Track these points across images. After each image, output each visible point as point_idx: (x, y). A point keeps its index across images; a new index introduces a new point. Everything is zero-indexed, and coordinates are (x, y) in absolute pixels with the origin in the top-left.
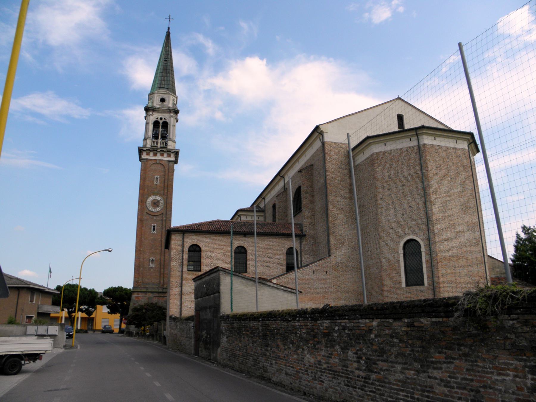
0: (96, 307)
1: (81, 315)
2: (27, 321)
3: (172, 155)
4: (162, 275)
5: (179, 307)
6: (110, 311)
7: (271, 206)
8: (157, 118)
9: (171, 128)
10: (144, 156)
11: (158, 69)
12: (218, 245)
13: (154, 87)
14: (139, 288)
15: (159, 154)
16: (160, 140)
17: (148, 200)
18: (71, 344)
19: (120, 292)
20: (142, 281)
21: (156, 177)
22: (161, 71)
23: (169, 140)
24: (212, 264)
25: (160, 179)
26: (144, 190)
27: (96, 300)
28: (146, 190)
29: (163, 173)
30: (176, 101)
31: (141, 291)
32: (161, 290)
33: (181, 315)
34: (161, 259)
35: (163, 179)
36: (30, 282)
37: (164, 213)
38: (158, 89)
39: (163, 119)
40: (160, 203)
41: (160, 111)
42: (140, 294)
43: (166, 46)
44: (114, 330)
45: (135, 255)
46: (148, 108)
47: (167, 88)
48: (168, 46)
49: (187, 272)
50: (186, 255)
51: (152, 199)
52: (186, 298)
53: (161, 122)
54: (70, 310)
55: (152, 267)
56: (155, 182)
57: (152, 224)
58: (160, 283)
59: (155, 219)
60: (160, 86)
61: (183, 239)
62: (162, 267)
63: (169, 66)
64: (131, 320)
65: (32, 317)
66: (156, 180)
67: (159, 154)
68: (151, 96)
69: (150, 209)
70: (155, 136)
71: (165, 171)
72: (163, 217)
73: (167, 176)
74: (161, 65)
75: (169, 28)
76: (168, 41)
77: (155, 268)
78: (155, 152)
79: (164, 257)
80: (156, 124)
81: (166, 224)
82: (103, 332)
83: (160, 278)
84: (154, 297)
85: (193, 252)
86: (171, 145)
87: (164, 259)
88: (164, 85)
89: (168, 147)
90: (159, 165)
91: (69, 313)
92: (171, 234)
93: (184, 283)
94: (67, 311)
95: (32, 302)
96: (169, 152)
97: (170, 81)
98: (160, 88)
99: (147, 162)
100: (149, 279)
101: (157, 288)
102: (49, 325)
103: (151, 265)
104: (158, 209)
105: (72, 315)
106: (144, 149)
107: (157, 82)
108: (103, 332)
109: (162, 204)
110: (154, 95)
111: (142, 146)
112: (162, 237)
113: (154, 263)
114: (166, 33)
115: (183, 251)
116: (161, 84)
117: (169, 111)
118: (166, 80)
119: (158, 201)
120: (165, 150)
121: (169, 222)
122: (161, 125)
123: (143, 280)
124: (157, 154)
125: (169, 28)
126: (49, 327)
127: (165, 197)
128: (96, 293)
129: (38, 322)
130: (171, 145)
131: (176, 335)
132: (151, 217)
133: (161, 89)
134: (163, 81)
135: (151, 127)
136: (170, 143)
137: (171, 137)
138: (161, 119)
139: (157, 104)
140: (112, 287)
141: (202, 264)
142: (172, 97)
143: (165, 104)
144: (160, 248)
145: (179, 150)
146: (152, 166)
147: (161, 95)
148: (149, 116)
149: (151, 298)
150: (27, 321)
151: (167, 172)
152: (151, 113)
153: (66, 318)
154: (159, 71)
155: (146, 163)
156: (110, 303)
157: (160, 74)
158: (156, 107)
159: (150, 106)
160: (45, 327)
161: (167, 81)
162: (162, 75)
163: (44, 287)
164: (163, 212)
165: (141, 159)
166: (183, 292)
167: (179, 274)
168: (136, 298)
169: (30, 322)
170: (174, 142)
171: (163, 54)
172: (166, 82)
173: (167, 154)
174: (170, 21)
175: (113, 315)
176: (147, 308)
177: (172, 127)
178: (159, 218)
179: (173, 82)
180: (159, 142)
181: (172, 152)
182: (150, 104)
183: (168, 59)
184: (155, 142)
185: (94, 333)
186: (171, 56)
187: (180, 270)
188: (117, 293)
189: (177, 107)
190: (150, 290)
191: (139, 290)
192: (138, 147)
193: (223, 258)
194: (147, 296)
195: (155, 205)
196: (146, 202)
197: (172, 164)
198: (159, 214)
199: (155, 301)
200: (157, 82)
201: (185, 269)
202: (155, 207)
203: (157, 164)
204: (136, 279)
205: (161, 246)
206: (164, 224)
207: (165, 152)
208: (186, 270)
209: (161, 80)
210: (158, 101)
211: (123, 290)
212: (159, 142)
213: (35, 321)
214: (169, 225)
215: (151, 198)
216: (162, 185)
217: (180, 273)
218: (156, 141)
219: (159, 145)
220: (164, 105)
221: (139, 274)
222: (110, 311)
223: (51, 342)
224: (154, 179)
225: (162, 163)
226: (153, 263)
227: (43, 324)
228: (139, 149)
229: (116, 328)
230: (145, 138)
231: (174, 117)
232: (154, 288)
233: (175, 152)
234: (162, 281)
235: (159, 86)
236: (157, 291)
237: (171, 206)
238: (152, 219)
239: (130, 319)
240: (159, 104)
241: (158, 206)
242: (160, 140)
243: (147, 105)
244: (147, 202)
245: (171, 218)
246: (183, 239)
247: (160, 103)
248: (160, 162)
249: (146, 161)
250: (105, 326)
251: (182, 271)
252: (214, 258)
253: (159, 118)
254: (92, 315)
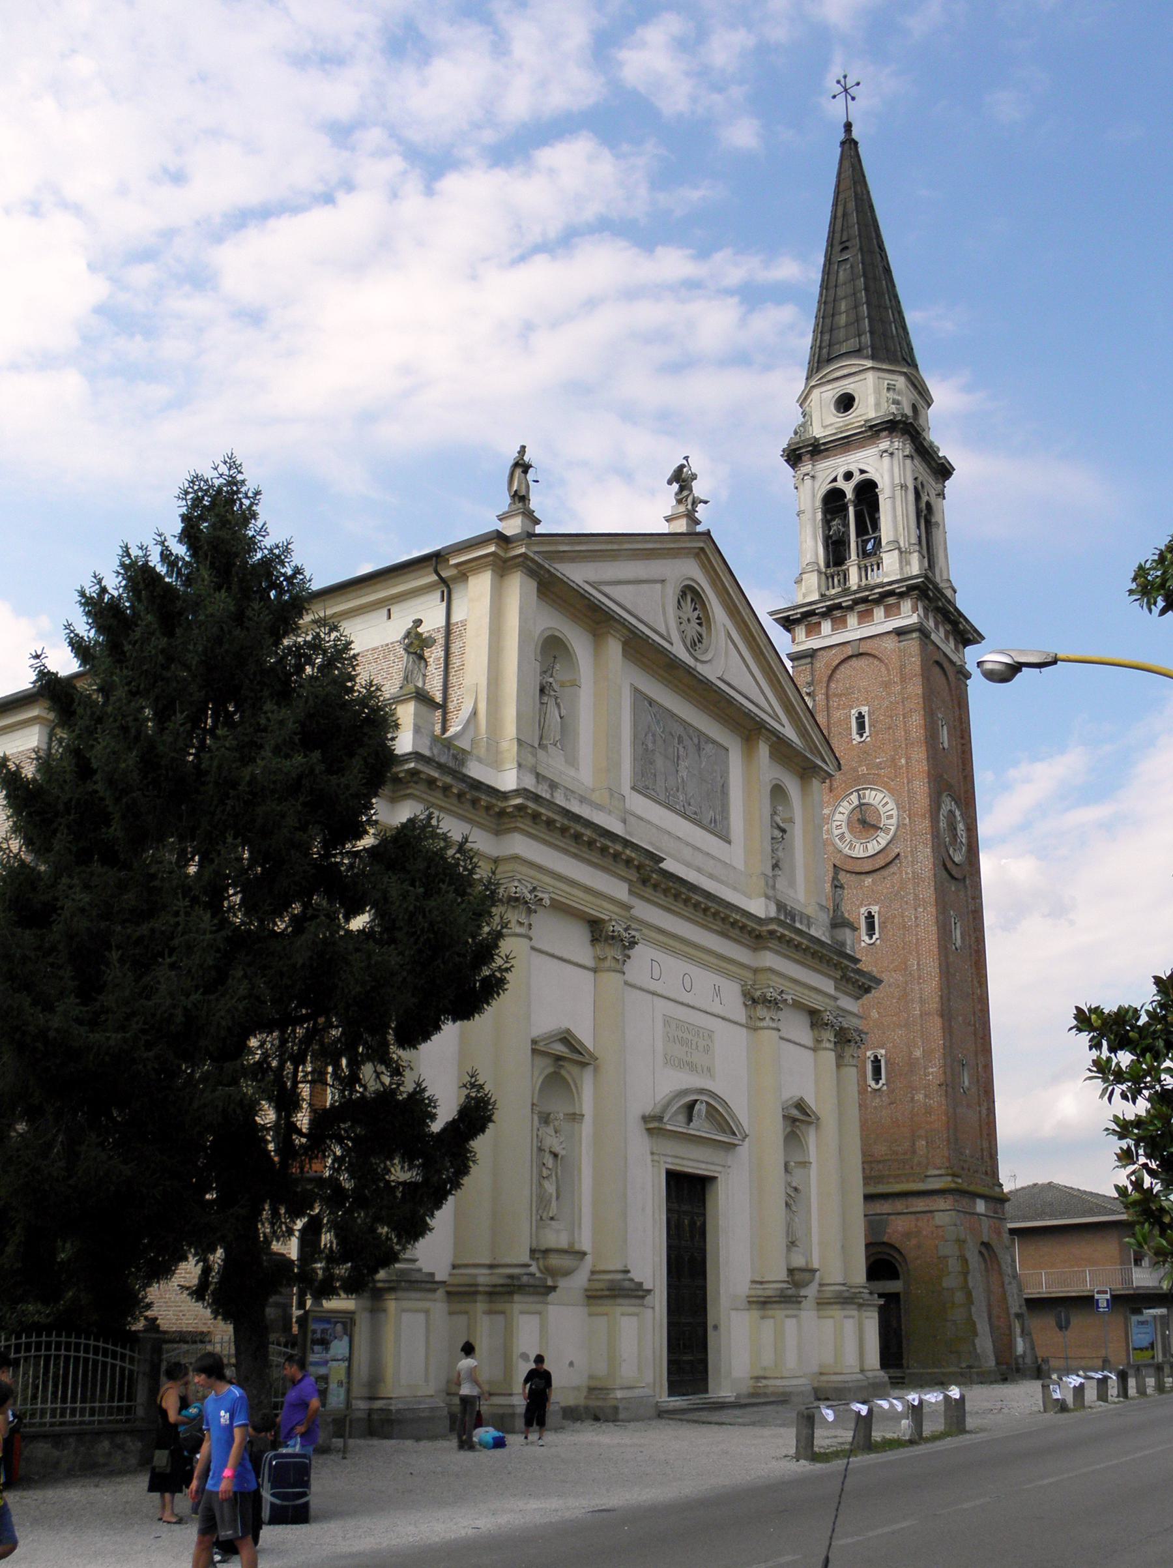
8: (835, 480)
53: (848, 488)
72: (829, 354)
80: (833, 501)
125: (848, 127)
138: (848, 476)
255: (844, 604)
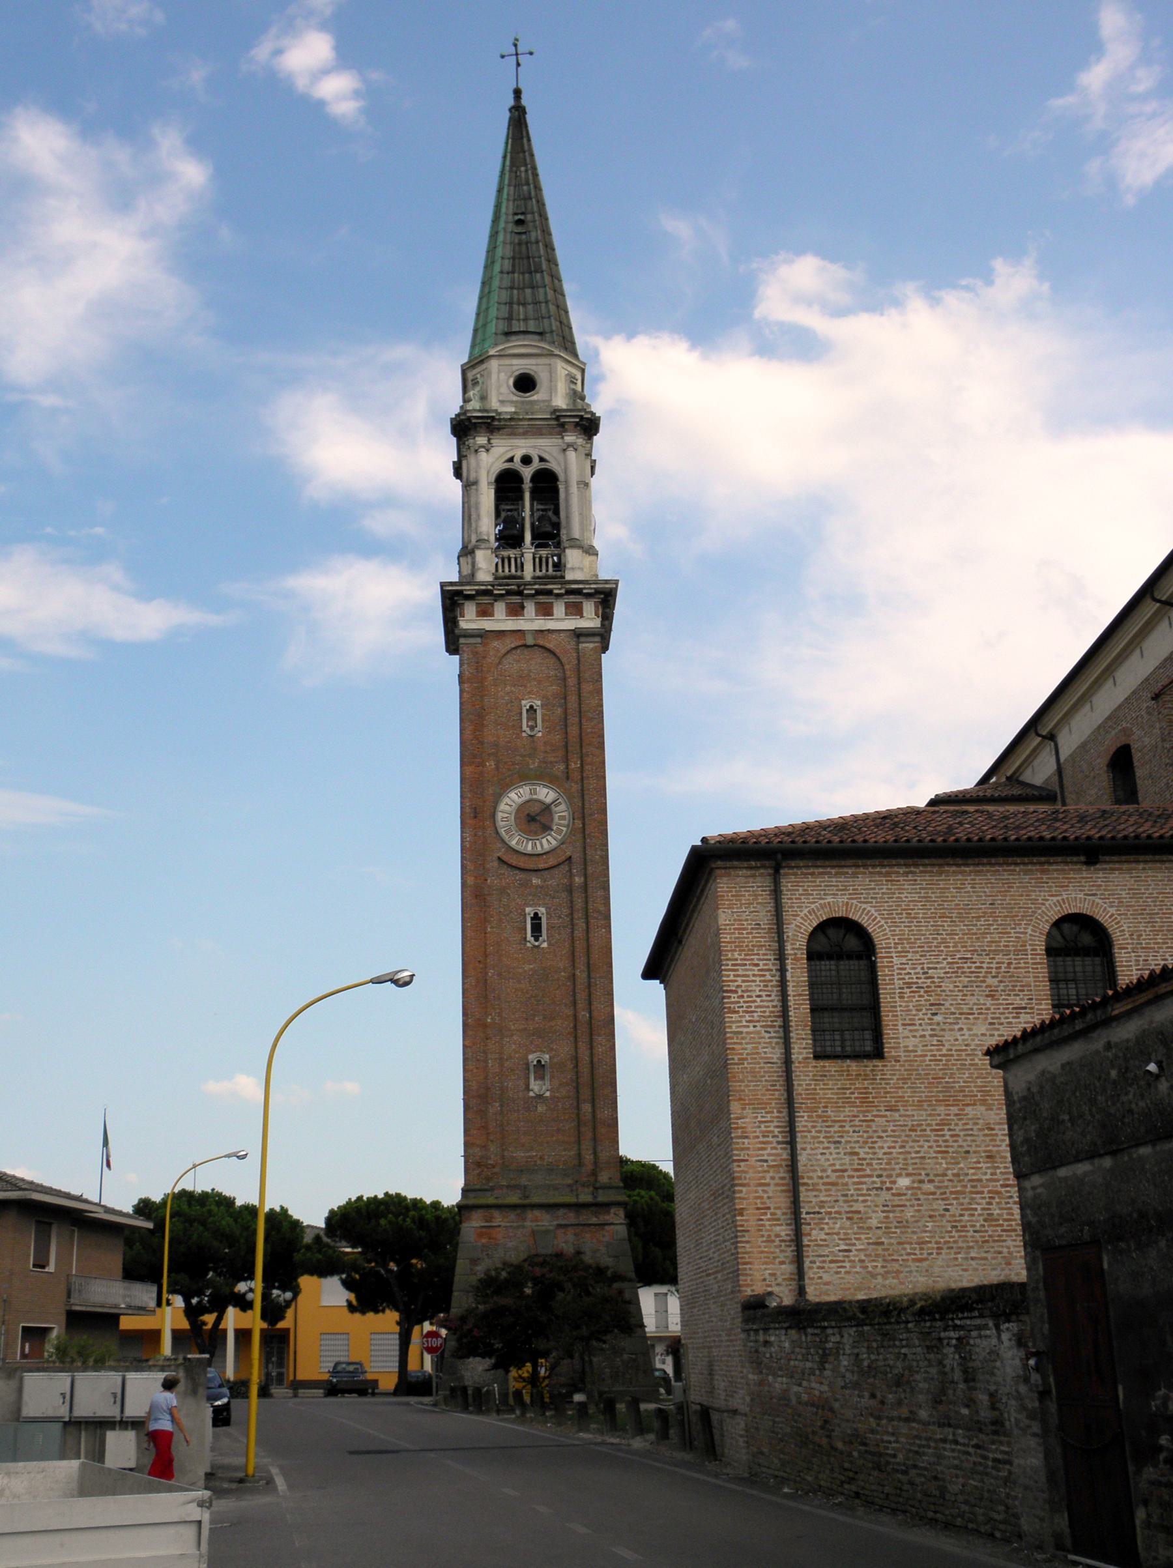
0: (298, 1286)
1: (236, 1321)
2: (27, 1350)
3: (589, 607)
4: (587, 1132)
5: (790, 1252)
6: (357, 1298)
7: (1102, 762)
8: (511, 460)
9: (570, 495)
10: (469, 620)
11: (493, 262)
12: (960, 916)
13: (484, 333)
14: (492, 1189)
15: (530, 608)
16: (528, 550)
17: (502, 806)
18: (239, 1461)
19: (397, 1216)
20: (503, 1157)
21: (526, 704)
22: (507, 265)
23: (571, 547)
24: (938, 1018)
25: (543, 715)
26: (482, 764)
27: (297, 1257)
28: (490, 764)
29: (555, 688)
30: (579, 382)
31: (500, 1202)
32: (586, 1197)
33: (801, 1291)
34: (576, 1059)
35: (559, 711)
36: (32, 1183)
37: (577, 857)
38: (503, 338)
39: (536, 460)
40: (556, 816)
41: (521, 431)
42: (498, 1219)
43: (512, 164)
44: (376, 1381)
45: (465, 1046)
46: (469, 419)
47: (540, 334)
48: (526, 165)
49: (814, 1063)
50: (798, 974)
51: (520, 801)
52: (822, 1204)
53: (527, 473)
54: (194, 1301)
55: (540, 1097)
56: (525, 727)
57: (528, 910)
58: (580, 1164)
59: (537, 886)
60: (510, 325)
61: (776, 893)
62: (585, 1093)
63: (537, 242)
64: (476, 1332)
65: (45, 1331)
66: (528, 719)
67: (530, 608)
68: (475, 371)
69: (513, 843)
70: (509, 538)
71: (565, 679)
72: (571, 876)
73: (573, 699)
74: (504, 243)
75: (517, 93)
76: (522, 145)
77: (552, 1097)
78: (516, 599)
79: (591, 1048)
80: (507, 484)
81: (587, 903)
82: (332, 1390)
83: (579, 1142)
84: (560, 1226)
85: (830, 957)
86: (576, 567)
87: (592, 1054)
88: (526, 319)
89: (569, 576)
90: (538, 656)
91: (192, 1312)
92: (712, 870)
93: (803, 1121)
94: (183, 1305)
95: (43, 1267)
96: (576, 595)
97: (547, 302)
98: (508, 334)
99: (484, 644)
100: (532, 1149)
101: (569, 1185)
102: (128, 1369)
103: (535, 1086)
104: (547, 842)
105: (205, 1323)
106: (469, 589)
107: (493, 312)
108: (332, 1390)
109: (563, 818)
110: (483, 366)
111: (455, 578)
112: (573, 961)
113: (547, 1077)
114: (508, 115)
115: (781, 957)
116: (510, 319)
117: (558, 422)
118: (529, 299)
119: (547, 809)
120: (557, 589)
121: (600, 893)
122: (527, 486)
123: (506, 1153)
124: (523, 607)
125: (517, 93)
126: (131, 1376)
127: (575, 787)
128: (296, 1224)
129: (73, 1353)
130: (576, 567)
131: (822, 1405)
132: (522, 875)
133: (513, 338)
134: (519, 304)
135: (487, 497)
136: (573, 557)
137: (576, 534)
138: (526, 460)
139: (502, 402)
140: (360, 1198)
141: (887, 1018)
142: (562, 369)
143: (535, 398)
144: (569, 1012)
145: (616, 582)
146: (510, 658)
147: (515, 361)
148: (476, 451)
149: (547, 1232)
150: (27, 1350)
151: (572, 682)
152: (481, 440)
153: (177, 1335)
154: (497, 268)
155: (480, 649)
156: (354, 1267)
157: (501, 279)
158: (500, 414)
159: (475, 410)
160: (109, 1380)
161: (536, 303)
162: (513, 281)
163: (86, 1201)
164: (568, 854)
165: (453, 641)
166: (801, 1168)
167: (771, 1074)
168: (480, 1235)
169: (37, 1352)
170: (591, 551)
171: (505, 196)
172: (530, 307)
173: (567, 605)
174: (518, 65)
175: (370, 1315)
176: (543, 1275)
177: (574, 489)
178: (556, 880)
179: (562, 309)
180: (528, 557)
181: (589, 596)
182: (474, 405)
183: (529, 217)
184: (509, 559)
185: (296, 1396)
186: (541, 204)
187: (776, 1054)
188: (383, 1222)
189: (589, 405)
190: (536, 1199)
191: (491, 1201)
192: (442, 585)
193: (990, 981)
194: (528, 1224)
195: (533, 826)
196: (493, 816)
197: (591, 645)
198: (552, 862)
199: (565, 1242)
200: (493, 312)
201: (802, 1048)
202: (536, 834)
203: (526, 651)
204: (477, 1150)
205: (575, 1003)
206: (579, 903)
207: (558, 596)
208: (808, 1053)
209: (511, 304)
210: (504, 390)
211: (407, 1208)
212: (528, 557)
213: (58, 1348)
214: (602, 908)
215: (515, 798)
216: (557, 738)
217: (778, 1068)
218: (512, 553)
219: (528, 572)
220: (532, 402)
221: (485, 1127)
222: (354, 1302)
223: (196, 1513)
224: (521, 714)
225: (550, 646)
226: (542, 1078)
227: (99, 1364)
228: (443, 592)
229: (384, 1371)
230: (464, 547)
231: (580, 448)
232: (556, 1188)
233: (598, 592)
234: (588, 1157)
235: (503, 326)
236: (570, 1199)
237: (604, 823)
238: (526, 884)
239: (470, 1331)
240: (512, 402)
241: (546, 828)
242: (528, 550)
243: (462, 407)
244: (500, 815)
245: (607, 875)
246: (776, 893)
247: (516, 397)
248: (541, 642)
249: (479, 640)
250: (337, 1364)
251: (787, 1061)
252: (948, 986)
253: (517, 459)
254: (282, 1318)
255: (465, 593)
